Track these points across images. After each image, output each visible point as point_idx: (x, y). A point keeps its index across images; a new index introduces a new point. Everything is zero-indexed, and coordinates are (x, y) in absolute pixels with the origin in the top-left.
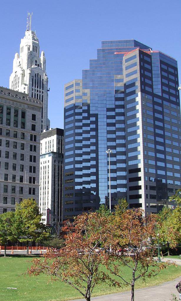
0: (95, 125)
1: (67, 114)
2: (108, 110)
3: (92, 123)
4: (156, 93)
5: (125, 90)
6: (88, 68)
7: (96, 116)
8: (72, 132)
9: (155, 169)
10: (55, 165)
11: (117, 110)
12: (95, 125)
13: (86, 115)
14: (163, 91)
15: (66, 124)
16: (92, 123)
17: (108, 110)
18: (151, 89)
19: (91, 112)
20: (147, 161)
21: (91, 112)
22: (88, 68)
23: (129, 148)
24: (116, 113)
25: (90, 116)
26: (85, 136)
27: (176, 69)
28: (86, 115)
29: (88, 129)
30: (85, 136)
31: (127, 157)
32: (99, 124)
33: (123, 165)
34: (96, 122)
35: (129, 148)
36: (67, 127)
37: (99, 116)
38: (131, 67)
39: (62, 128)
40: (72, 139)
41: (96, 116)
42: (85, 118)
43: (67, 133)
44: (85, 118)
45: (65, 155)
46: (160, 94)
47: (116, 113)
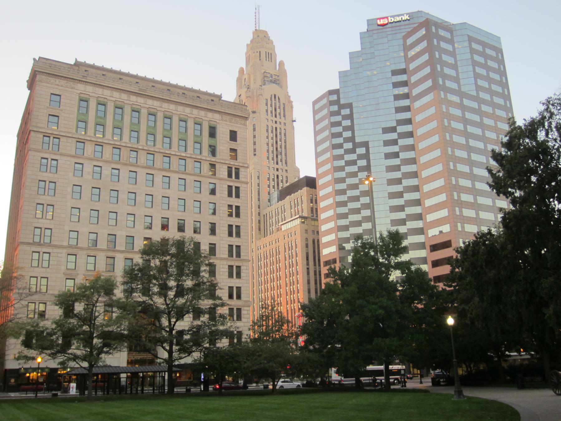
0: (364, 149)
1: (320, 160)
2: (386, 130)
3: (360, 157)
4: (468, 92)
5: (408, 66)
6: (347, 67)
7: (366, 145)
8: (329, 178)
9: (464, 124)
10: (307, 239)
11: (400, 129)
12: (364, 149)
13: (349, 145)
14: (479, 88)
15: (318, 166)
16: (360, 157)
17: (386, 130)
18: (454, 72)
19: (357, 140)
20: (461, 227)
21: (357, 140)
22: (347, 67)
23: (428, 220)
24: (399, 134)
25: (355, 145)
26: (351, 205)
27: (499, 51)
28: (349, 145)
29: (357, 205)
30: (351, 205)
31: (425, 223)
32: (372, 157)
33: (420, 239)
34: (366, 156)
35: (428, 220)
36: (321, 170)
37: (370, 145)
38: (419, 66)
39: (313, 174)
40: (331, 225)
41: (366, 145)
42: (348, 152)
43: (320, 182)
44: (348, 152)
45: (322, 241)
46: (474, 93)
47: (399, 134)
